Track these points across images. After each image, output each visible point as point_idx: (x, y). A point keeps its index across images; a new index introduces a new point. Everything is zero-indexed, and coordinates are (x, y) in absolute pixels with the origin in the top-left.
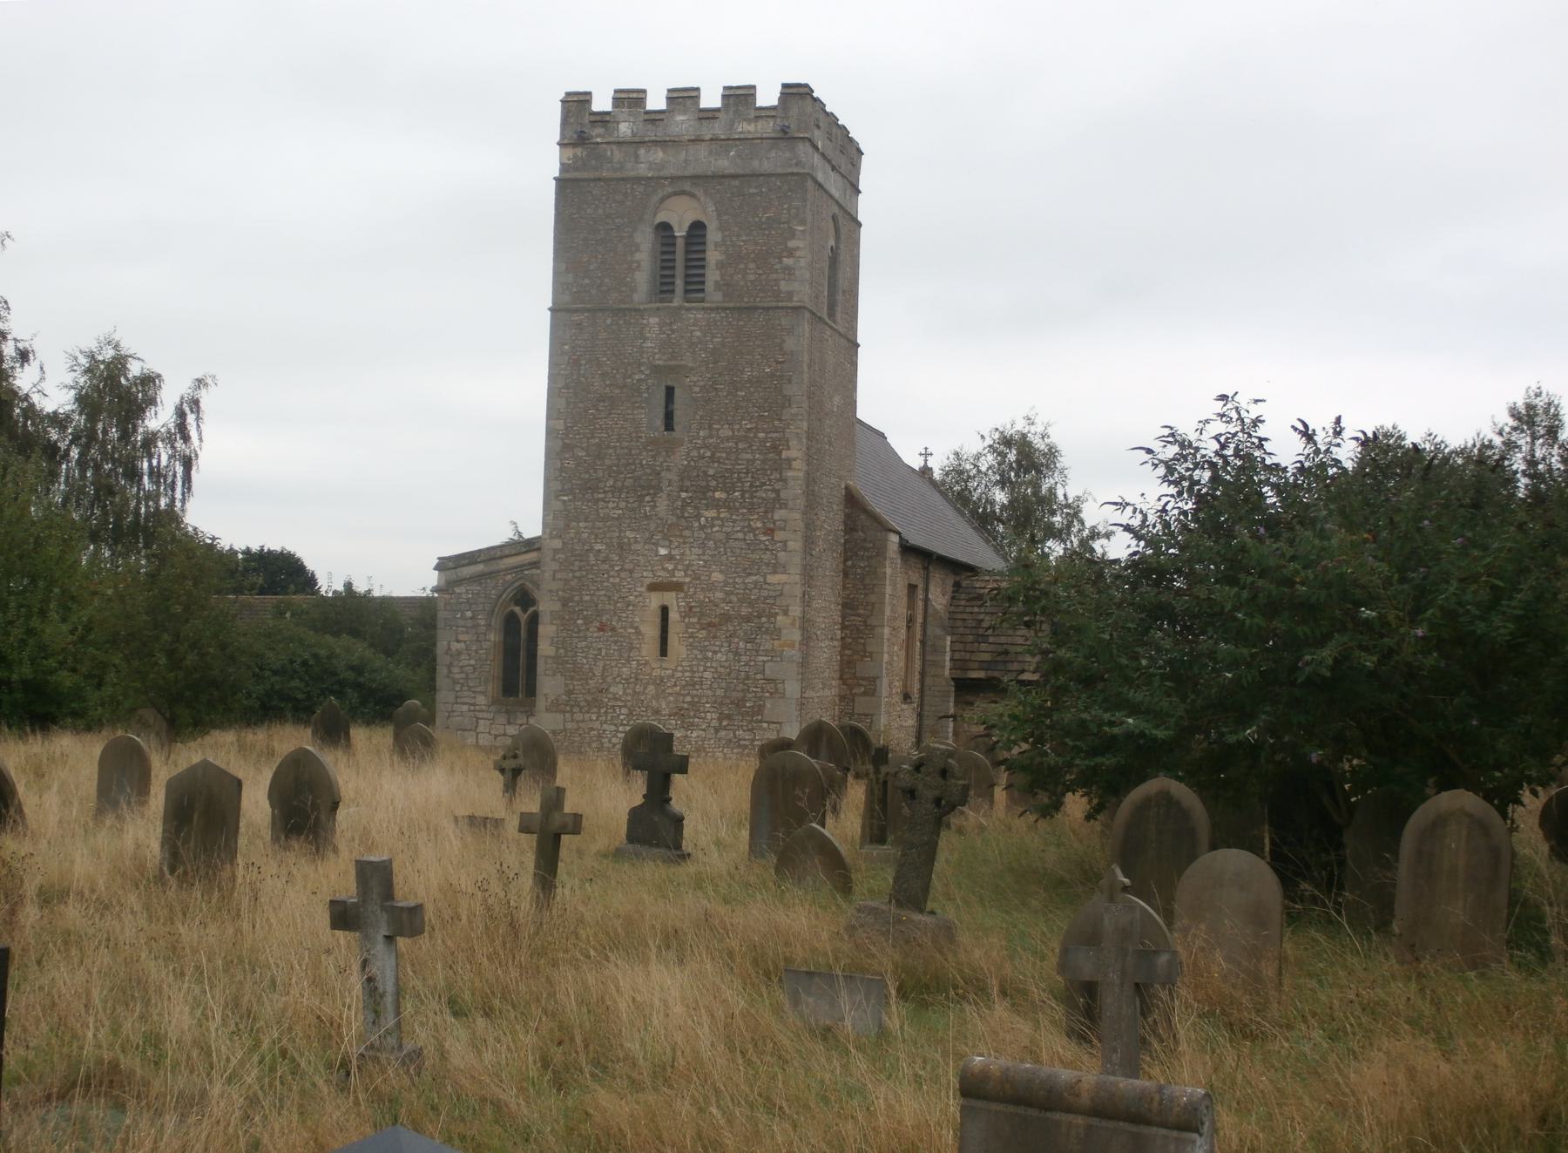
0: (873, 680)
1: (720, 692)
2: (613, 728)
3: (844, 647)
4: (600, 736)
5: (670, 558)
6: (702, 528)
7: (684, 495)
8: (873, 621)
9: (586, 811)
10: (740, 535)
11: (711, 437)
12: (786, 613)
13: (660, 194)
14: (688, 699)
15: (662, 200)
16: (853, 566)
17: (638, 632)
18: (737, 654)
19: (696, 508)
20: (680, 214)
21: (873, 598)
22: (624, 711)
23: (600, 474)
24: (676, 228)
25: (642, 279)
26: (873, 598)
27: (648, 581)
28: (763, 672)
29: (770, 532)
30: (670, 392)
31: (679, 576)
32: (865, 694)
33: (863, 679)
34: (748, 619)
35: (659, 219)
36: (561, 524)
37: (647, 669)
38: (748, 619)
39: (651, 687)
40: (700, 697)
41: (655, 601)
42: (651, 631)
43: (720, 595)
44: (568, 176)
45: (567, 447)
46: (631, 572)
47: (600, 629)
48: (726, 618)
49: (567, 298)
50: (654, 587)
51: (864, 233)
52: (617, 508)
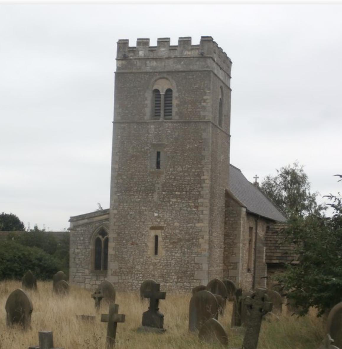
0: (236, 264)
2: (137, 282)
4: (132, 285)
5: (158, 217)
6: (171, 205)
8: (236, 241)
10: (185, 208)
11: (174, 171)
13: (155, 78)
14: (165, 271)
15: (156, 81)
19: (169, 198)
24: (161, 91)
27: (150, 226)
28: (194, 261)
30: (158, 154)
31: (162, 224)
32: (233, 269)
33: (232, 263)
34: (188, 240)
35: (155, 87)
37: (150, 260)
41: (153, 233)
42: (151, 245)
43: (177, 231)
47: (132, 244)
48: (180, 240)
50: (153, 228)
51: (233, 94)
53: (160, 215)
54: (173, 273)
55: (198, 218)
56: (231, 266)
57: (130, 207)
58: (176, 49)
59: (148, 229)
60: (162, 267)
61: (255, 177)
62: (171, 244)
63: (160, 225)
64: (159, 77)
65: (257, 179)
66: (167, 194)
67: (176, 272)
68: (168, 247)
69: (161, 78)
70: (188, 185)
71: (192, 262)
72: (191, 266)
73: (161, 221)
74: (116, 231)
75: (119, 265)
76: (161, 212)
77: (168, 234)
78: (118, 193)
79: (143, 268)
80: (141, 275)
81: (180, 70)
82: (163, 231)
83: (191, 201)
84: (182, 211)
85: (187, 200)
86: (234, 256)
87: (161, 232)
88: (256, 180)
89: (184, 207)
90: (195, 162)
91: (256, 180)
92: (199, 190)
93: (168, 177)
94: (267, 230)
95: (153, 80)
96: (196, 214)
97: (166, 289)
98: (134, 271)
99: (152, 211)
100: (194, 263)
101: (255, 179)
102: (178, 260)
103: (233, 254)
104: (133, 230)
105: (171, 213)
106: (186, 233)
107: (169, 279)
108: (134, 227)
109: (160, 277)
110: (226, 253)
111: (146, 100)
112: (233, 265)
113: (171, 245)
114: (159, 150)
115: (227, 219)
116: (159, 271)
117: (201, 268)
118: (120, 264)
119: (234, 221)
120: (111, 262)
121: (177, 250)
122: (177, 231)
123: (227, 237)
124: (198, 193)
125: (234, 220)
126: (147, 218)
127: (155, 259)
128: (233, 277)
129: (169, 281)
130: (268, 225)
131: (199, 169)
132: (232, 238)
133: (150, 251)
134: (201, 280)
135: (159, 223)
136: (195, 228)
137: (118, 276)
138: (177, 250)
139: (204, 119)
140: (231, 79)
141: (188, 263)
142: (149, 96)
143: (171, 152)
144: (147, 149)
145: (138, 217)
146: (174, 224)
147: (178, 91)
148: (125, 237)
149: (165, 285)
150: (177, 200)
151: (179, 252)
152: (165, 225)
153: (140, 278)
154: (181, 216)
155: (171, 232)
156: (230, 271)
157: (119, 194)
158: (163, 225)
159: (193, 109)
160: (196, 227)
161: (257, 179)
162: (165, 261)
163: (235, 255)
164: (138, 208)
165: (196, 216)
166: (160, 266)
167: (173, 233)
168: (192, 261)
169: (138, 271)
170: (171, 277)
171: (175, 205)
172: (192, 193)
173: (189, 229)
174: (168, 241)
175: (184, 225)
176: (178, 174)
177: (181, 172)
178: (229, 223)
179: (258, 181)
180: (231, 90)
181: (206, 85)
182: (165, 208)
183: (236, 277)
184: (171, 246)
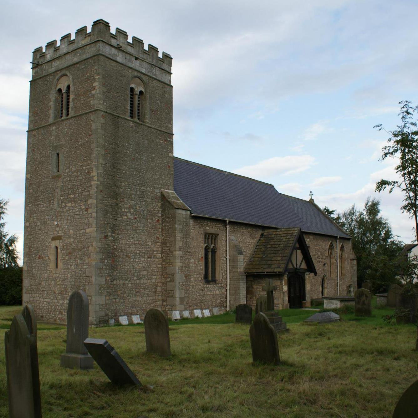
0: (173, 275)
1: (73, 283)
2: (42, 300)
3: (163, 261)
4: (39, 304)
5: (58, 225)
6: (67, 211)
7: (62, 198)
8: (172, 249)
9: (291, 329)
10: (78, 213)
11: (69, 172)
12: (92, 245)
13: (57, 77)
14: (63, 286)
15: (58, 80)
16: (165, 226)
17: (49, 259)
18: (77, 265)
19: (65, 203)
20: (63, 85)
21: (172, 239)
22: (46, 292)
23: (39, 194)
24: (63, 90)
25: (52, 113)
26: (172, 239)
27: (52, 236)
28: (85, 273)
29: (87, 210)
30: (58, 154)
31: (60, 234)
32: (170, 281)
33: (170, 275)
34: (80, 250)
35: (58, 87)
36: (29, 215)
37: (51, 274)
38: (80, 250)
39: (53, 282)
40: (67, 285)
41: (54, 244)
42: (53, 258)
43: (72, 240)
44: (34, 79)
45: (31, 184)
46: (47, 233)
47: (39, 258)
48: (74, 250)
49: (32, 126)
50: (54, 239)
51: (174, 89)
52: (44, 207)
53: (59, 223)
54: (69, 289)
55: (88, 223)
56: (169, 277)
57: (38, 217)
58: (74, 42)
59: (50, 240)
60: (60, 282)
61: (310, 194)
62: (67, 255)
63: (59, 235)
64: (60, 75)
65: (312, 196)
66: (64, 199)
67: (71, 288)
68: (65, 259)
69: (62, 76)
70: (80, 185)
71: (84, 275)
72: (83, 280)
73: (59, 230)
74: (28, 245)
75: (30, 282)
76: (59, 219)
77: (65, 244)
78: (30, 204)
79: (47, 284)
80: (46, 292)
81: (78, 61)
82: (61, 241)
83: (83, 204)
84: (76, 217)
85: (79, 203)
86: (171, 266)
87: (60, 243)
88: (311, 197)
89: (77, 211)
90: (86, 158)
91: (311, 197)
92: (89, 189)
93: (65, 180)
94: (260, 237)
95: (55, 80)
96: (86, 218)
97: (64, 307)
98: (41, 288)
99: (53, 219)
100: (86, 276)
101: (310, 196)
102: (73, 273)
103: (170, 265)
104: (40, 243)
105: (67, 220)
106: (78, 242)
107: (66, 296)
108: (40, 239)
109: (60, 293)
110: (164, 263)
111: (51, 101)
112: (170, 276)
113: (67, 256)
114: (58, 152)
115: (163, 225)
116: (59, 286)
117: (91, 281)
118: (31, 281)
119: (170, 226)
120: (25, 278)
121: (72, 261)
122: (72, 240)
123: (164, 245)
124: (88, 193)
125: (170, 225)
126: (49, 228)
127: (55, 273)
128: (171, 291)
129: (66, 298)
130: (263, 232)
131: (89, 165)
132: (168, 245)
133: (52, 265)
134: (91, 296)
135: (58, 232)
136: (86, 234)
137: (30, 293)
138: (72, 261)
139: (94, 108)
140: (172, 75)
141: (81, 277)
142: (53, 96)
143: (67, 152)
144: (50, 153)
145: (43, 228)
146: (69, 232)
147: (73, 86)
148: (34, 251)
149: (63, 303)
150: (72, 204)
151: (73, 264)
152: (63, 234)
153: (45, 295)
154: (75, 221)
155: (67, 241)
156: (168, 283)
157: (30, 205)
158: (61, 235)
159: (85, 100)
160: (87, 233)
161: (312, 196)
162: (63, 275)
163: (172, 265)
164: (43, 218)
165: (86, 221)
166: (60, 281)
167: (68, 243)
168: (83, 274)
169: (43, 287)
170: (68, 293)
171: (70, 210)
172: (83, 194)
173: (81, 236)
174: (64, 252)
175: (77, 233)
176: (73, 175)
177: (74, 172)
178: (166, 229)
179: (313, 198)
180: (172, 87)
181: (95, 71)
182: (62, 214)
183: (173, 290)
184: (67, 258)
